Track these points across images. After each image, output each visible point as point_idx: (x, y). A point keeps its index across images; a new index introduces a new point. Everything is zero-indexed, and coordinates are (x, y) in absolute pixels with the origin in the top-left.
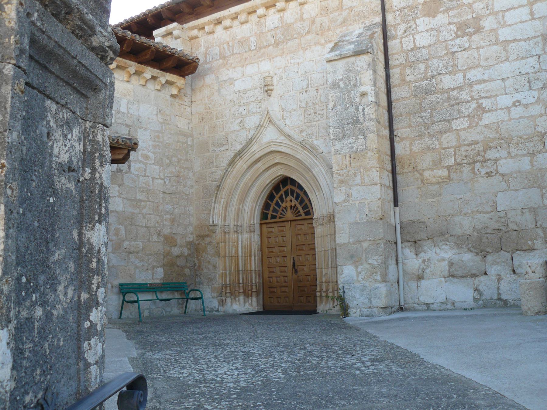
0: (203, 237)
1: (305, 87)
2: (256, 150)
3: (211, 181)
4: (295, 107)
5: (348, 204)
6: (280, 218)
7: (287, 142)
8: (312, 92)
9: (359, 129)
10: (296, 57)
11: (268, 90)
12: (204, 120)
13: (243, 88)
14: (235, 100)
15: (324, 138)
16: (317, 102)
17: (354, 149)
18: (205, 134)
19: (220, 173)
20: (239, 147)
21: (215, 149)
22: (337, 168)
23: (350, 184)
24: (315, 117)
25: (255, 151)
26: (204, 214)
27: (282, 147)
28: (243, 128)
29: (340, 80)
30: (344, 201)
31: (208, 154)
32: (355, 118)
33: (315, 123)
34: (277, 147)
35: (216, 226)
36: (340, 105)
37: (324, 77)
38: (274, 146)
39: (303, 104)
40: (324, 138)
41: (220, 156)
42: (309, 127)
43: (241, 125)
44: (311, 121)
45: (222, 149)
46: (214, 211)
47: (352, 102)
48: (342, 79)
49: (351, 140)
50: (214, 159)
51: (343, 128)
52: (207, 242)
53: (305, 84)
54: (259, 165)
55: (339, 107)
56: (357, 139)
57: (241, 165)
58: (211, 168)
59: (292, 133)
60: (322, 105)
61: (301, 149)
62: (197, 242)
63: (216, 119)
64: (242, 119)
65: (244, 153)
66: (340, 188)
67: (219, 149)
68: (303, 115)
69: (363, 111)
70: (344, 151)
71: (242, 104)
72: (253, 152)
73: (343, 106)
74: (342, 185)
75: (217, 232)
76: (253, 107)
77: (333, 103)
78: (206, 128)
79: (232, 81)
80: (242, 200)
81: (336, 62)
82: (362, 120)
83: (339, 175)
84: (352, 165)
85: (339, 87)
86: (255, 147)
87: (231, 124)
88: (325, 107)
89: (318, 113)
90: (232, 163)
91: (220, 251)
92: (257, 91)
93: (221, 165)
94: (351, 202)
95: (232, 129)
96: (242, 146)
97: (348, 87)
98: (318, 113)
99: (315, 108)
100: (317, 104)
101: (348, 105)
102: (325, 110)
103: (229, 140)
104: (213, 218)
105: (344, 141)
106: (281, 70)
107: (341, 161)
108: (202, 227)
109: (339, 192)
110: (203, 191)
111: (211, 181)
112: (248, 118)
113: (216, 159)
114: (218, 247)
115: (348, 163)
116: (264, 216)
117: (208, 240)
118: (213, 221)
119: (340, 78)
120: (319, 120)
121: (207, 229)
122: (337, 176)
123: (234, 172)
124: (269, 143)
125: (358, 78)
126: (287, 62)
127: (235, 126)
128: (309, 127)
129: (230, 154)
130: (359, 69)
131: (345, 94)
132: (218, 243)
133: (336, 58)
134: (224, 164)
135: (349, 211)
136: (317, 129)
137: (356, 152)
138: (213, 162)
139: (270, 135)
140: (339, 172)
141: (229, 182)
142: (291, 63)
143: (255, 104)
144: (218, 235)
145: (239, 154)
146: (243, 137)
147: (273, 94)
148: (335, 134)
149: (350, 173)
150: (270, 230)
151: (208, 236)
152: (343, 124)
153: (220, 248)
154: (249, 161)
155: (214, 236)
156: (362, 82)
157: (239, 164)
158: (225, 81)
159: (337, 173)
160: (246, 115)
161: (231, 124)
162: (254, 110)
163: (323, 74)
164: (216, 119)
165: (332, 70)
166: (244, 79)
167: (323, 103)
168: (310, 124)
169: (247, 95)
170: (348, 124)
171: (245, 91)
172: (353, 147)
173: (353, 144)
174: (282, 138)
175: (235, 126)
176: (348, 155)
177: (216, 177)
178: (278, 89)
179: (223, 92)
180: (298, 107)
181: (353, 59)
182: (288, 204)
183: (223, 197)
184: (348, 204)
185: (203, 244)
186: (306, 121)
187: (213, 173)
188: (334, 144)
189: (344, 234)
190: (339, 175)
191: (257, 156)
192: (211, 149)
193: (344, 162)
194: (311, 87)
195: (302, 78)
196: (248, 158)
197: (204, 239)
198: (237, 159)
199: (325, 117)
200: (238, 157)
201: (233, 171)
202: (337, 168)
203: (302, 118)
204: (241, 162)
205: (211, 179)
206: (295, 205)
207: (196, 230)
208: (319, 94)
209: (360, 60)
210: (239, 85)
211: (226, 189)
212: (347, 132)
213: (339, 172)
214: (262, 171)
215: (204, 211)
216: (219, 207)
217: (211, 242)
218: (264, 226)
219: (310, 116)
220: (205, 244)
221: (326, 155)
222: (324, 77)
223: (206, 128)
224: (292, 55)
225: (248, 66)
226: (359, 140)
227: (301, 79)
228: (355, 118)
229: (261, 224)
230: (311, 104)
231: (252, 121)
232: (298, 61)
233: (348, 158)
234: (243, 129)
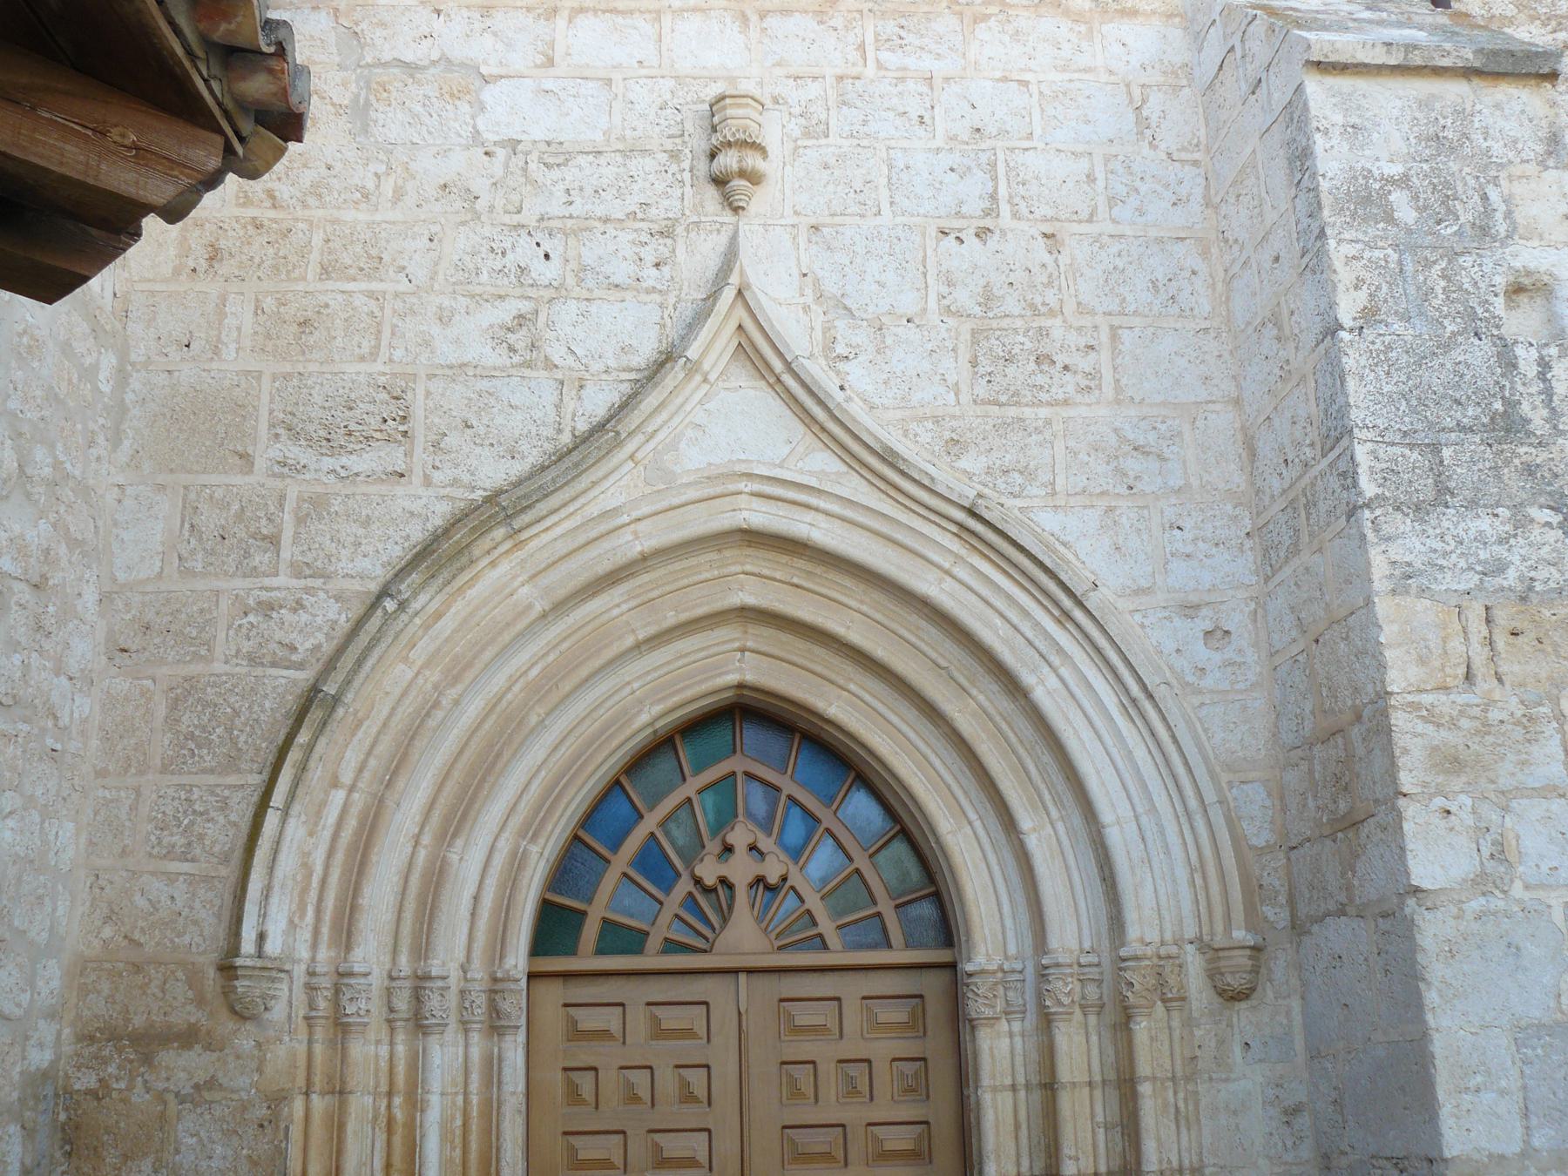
0: (147, 1044)
1: (974, 206)
2: (625, 501)
3: (253, 660)
4: (908, 303)
5: (1498, 903)
6: (671, 946)
7: (855, 488)
8: (1019, 243)
9: (1529, 470)
10: (910, 38)
11: (726, 167)
12: (224, 268)
13: (538, 134)
14: (480, 186)
15: (1103, 503)
16: (1052, 301)
17: (1511, 577)
18: (229, 353)
19: (327, 616)
20: (493, 472)
21: (297, 453)
22: (1414, 673)
23: (1505, 782)
24: (1041, 379)
25: (615, 511)
26: (171, 878)
27: (810, 516)
28: (533, 358)
29: (1391, 181)
30: (1481, 883)
31: (238, 480)
32: (1498, 406)
33: (1044, 412)
34: (783, 510)
35: (274, 970)
36: (1406, 318)
37: (1091, 178)
38: (757, 503)
39: (964, 298)
40: (1103, 503)
41: (336, 505)
42: (1002, 427)
43: (519, 339)
44: (1015, 399)
45: (361, 463)
46: (271, 869)
47: (1474, 317)
48: (1403, 181)
49: (1484, 524)
50: (288, 518)
51: (1435, 448)
52: (182, 1082)
53: (972, 191)
54: (612, 601)
55: (1398, 327)
56: (1521, 522)
57: (502, 579)
58: (254, 572)
59: (915, 449)
60: (1087, 321)
61: (955, 546)
62: (88, 1080)
63: (326, 272)
64: (525, 307)
65: (542, 508)
66: (1439, 802)
67: (328, 463)
68: (964, 355)
69: (1542, 376)
70: (1448, 582)
71: (529, 217)
72: (605, 515)
73: (1420, 326)
74: (1457, 783)
75: (278, 1012)
76: (615, 253)
77: (1362, 297)
78: (241, 315)
79: (466, 81)
80: (454, 821)
81: (1361, 84)
82: (1538, 419)
83: (1432, 717)
84: (1504, 668)
85: (1390, 218)
86: (617, 488)
87: (444, 318)
88: (1104, 336)
89: (1061, 359)
90: (438, 555)
91: (294, 1152)
92: (637, 164)
93: (344, 566)
94: (1517, 890)
95: (447, 353)
96: (518, 468)
97: (1448, 230)
98: (1061, 359)
99: (1043, 333)
100: (1052, 313)
101: (1451, 328)
102: (1105, 355)
103: (418, 412)
104: (263, 915)
105: (1448, 520)
106: (814, 89)
107: (1434, 641)
108: (137, 968)
109: (1437, 820)
110: (172, 721)
111: (253, 660)
112: (567, 312)
113: (301, 520)
114: (272, 1123)
115: (1479, 655)
116: (555, 926)
117: (182, 1067)
118: (262, 937)
119: (1395, 170)
120: (1066, 402)
121: (180, 991)
122: (1420, 727)
123: (447, 625)
124: (724, 482)
125: (1494, 194)
126: (854, 56)
127: (471, 337)
128: (1002, 427)
129: (424, 506)
130: (1497, 148)
131: (1428, 265)
132: (276, 1100)
133: (1378, 57)
134: (368, 564)
135: (1514, 949)
136: (1060, 445)
137: (1523, 599)
138: (274, 541)
139: (725, 436)
140: (1427, 699)
141: (390, 684)
142: (880, 66)
143: (625, 237)
144: (284, 1037)
145: (500, 511)
146: (531, 416)
147: (760, 202)
148: (1388, 475)
149: (1494, 715)
150: (672, 1018)
151: (188, 1037)
152: (1431, 425)
153: (296, 1132)
154: (563, 568)
155: (246, 1044)
156: (1518, 216)
157: (494, 574)
158: (411, 68)
159: (1416, 706)
160: (558, 291)
161: (444, 318)
162: (621, 271)
163: (1084, 164)
164: (326, 272)
165: (1339, 118)
166: (549, 84)
167: (1093, 313)
168: (1012, 412)
169: (570, 174)
170: (1461, 428)
171: (558, 154)
172: (1500, 567)
173: (1500, 551)
174: (819, 465)
175: (471, 337)
176: (1475, 613)
177: (294, 637)
178: (787, 185)
179: (391, 124)
180: (932, 303)
181: (1454, 91)
182: (741, 870)
183: (347, 778)
184: (1498, 903)
185: (139, 1097)
186: (982, 390)
187: (267, 608)
188: (1387, 529)
189: (1488, 1097)
190: (1432, 717)
191: (631, 545)
192: (266, 453)
193: (1456, 644)
194: (1016, 215)
195: (955, 159)
196: (562, 548)
197: (147, 1060)
198: (486, 543)
199: (1108, 391)
200: (499, 533)
201: (438, 616)
202: (1414, 673)
203: (955, 368)
204: (504, 567)
205: (246, 646)
206: (784, 879)
207: (84, 991)
208: (1064, 260)
209: (1497, 106)
210: (510, 110)
211: (370, 728)
212: (1461, 474)
213: (1427, 699)
214: (629, 641)
215: (169, 855)
216: (300, 843)
217: (211, 1083)
218: (552, 994)
219: (1011, 370)
220: (160, 1097)
221: (1121, 604)
222: (1091, 178)
223: (241, 315)
224: (890, 27)
225: (585, 21)
226: (1536, 533)
227: (947, 160)
228: (1498, 406)
229: (532, 976)
230: (1012, 305)
231: (610, 333)
232: (927, 63)
233: (1477, 628)
234: (528, 365)
